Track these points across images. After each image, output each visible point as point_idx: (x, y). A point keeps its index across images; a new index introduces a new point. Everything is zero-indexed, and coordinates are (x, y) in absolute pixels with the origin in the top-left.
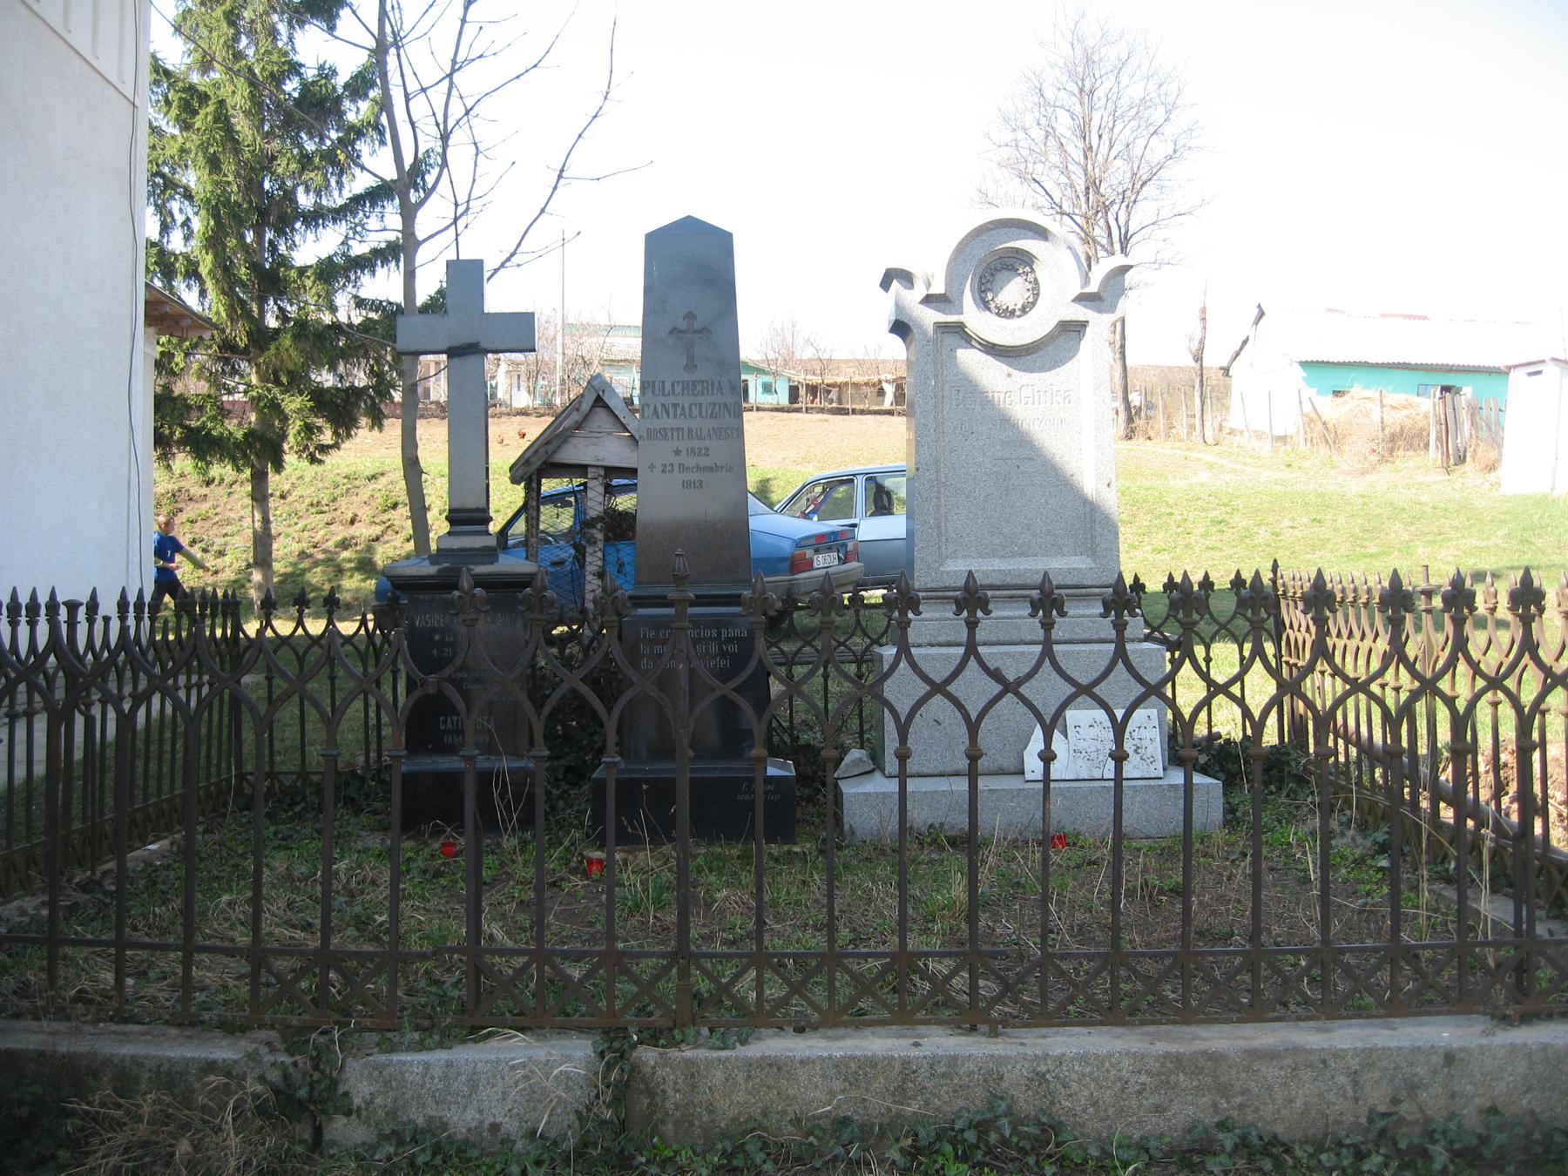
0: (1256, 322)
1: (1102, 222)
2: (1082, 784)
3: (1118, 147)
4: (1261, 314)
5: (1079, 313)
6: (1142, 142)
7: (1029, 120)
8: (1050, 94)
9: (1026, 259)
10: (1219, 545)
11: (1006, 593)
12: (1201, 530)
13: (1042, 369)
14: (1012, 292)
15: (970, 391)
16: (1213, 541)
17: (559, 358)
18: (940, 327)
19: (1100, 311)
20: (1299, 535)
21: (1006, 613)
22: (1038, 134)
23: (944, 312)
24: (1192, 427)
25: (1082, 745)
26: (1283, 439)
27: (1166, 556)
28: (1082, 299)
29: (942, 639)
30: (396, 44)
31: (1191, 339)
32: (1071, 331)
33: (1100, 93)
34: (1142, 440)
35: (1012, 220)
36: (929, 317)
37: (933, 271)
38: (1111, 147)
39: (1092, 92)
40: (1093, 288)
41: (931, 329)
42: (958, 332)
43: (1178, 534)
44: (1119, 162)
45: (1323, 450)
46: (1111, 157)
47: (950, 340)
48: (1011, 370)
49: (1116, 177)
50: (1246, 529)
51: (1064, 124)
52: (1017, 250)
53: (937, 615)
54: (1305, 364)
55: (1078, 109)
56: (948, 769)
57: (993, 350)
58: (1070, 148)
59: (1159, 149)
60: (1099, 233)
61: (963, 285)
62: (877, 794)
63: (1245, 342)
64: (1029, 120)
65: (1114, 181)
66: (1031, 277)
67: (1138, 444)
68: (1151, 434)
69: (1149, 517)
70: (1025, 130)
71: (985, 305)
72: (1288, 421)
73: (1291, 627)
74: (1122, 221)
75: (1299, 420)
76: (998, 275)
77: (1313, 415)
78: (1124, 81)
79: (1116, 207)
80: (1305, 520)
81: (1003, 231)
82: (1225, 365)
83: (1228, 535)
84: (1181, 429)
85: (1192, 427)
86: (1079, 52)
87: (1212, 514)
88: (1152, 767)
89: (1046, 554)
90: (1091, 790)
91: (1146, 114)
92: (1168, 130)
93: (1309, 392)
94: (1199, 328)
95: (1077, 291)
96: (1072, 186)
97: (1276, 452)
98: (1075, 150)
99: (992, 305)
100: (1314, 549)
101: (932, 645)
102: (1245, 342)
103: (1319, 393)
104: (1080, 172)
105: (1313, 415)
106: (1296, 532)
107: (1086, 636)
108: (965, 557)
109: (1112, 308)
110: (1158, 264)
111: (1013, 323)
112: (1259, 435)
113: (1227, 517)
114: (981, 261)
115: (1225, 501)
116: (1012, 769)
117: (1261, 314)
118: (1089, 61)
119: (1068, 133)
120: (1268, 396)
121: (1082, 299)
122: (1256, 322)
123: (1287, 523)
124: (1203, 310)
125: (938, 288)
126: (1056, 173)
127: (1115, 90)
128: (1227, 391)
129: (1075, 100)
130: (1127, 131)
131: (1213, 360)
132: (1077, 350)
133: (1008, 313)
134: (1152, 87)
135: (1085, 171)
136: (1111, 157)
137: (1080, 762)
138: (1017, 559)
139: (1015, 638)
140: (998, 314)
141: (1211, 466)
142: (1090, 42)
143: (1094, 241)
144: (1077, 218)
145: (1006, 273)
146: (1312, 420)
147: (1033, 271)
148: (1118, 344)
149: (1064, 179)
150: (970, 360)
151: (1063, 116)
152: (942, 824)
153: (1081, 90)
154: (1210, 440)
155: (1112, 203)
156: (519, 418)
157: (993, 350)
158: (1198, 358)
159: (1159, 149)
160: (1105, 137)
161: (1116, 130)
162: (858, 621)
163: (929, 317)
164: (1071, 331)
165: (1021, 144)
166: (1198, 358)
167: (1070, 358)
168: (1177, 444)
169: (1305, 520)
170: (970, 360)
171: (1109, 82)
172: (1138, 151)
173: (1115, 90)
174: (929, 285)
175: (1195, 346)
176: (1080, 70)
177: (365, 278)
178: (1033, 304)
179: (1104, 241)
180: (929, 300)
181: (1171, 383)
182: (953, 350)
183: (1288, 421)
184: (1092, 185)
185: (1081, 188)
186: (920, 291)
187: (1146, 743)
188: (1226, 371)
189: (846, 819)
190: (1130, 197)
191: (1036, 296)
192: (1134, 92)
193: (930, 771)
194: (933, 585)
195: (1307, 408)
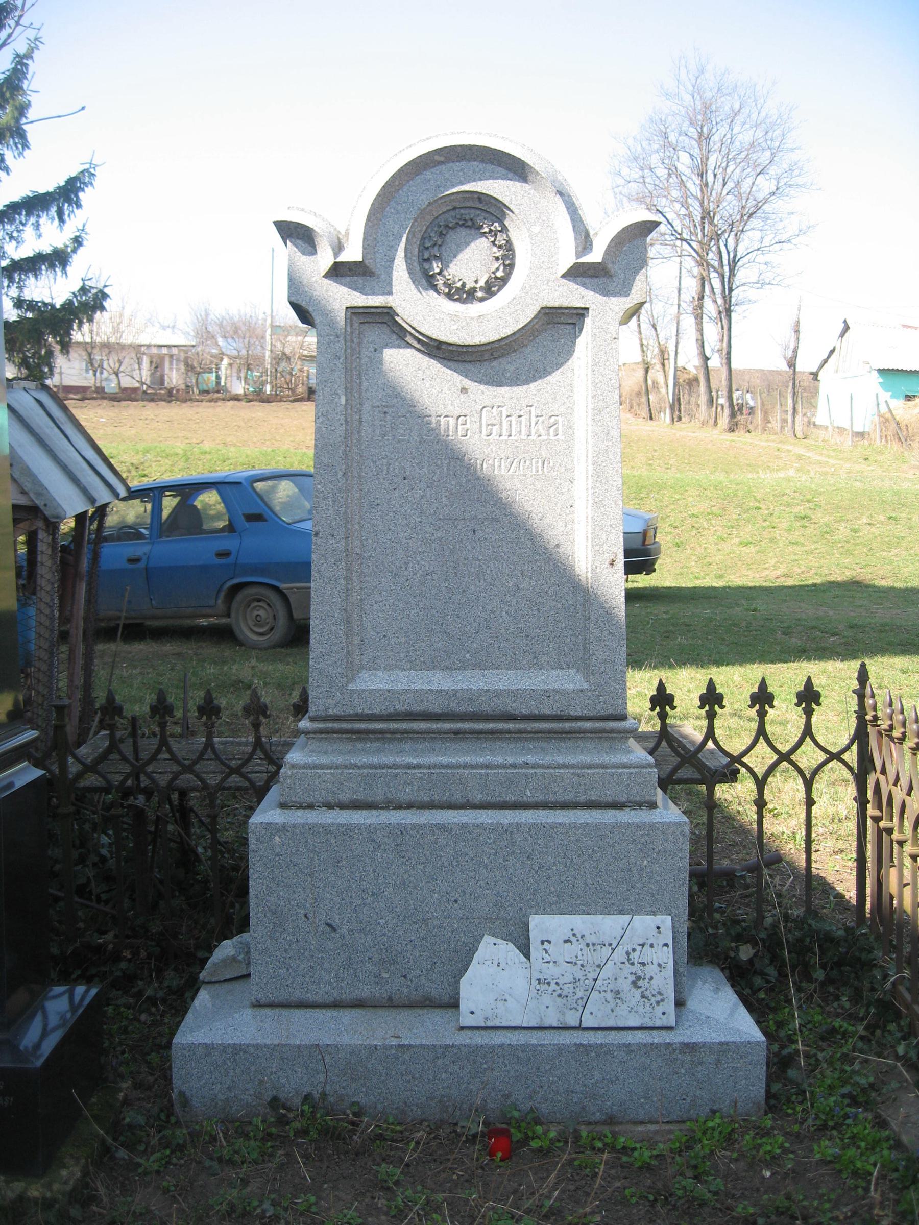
0: (842, 335)
1: (714, 249)
2: (547, 1038)
3: (730, 185)
4: (847, 328)
5: (574, 295)
6: (749, 181)
7: (654, 160)
8: (672, 138)
9: (494, 210)
10: (802, 540)
11: (448, 726)
12: (785, 525)
13: (517, 380)
14: (472, 261)
15: (401, 410)
16: (796, 536)
17: (268, 354)
18: (354, 312)
19: (606, 293)
20: (877, 532)
21: (444, 760)
22: (662, 172)
23: (362, 291)
24: (785, 421)
25: (551, 971)
26: (862, 435)
27: (752, 549)
28: (579, 273)
29: (345, 797)
30: (720, 313)
31: (786, 348)
32: (558, 326)
33: (716, 138)
34: (742, 432)
35: (471, 148)
36: (341, 298)
37: (345, 222)
38: (724, 185)
39: (708, 138)
40: (596, 256)
41: (341, 316)
42: (385, 319)
43: (764, 528)
44: (729, 197)
45: (896, 446)
46: (725, 192)
47: (373, 334)
48: (467, 383)
49: (729, 207)
50: (827, 526)
51: (684, 163)
52: (480, 197)
53: (339, 760)
54: (882, 372)
55: (696, 152)
56: (346, 997)
57: (436, 349)
58: (689, 185)
59: (765, 185)
60: (712, 257)
61: (393, 248)
62: (224, 1048)
63: (832, 352)
64: (654, 160)
65: (726, 214)
66: (501, 239)
67: (740, 437)
68: (751, 427)
69: (738, 511)
70: (651, 170)
71: (428, 281)
72: (865, 421)
73: (884, 772)
74: (731, 248)
75: (876, 419)
76: (452, 236)
77: (888, 416)
78: (737, 129)
79: (726, 235)
80: (882, 518)
81: (457, 166)
82: (814, 370)
83: (808, 532)
84: (775, 424)
85: (785, 421)
86: (698, 103)
87: (796, 510)
88: (659, 1010)
89: (514, 665)
90: (560, 1050)
91: (754, 156)
92: (773, 170)
93: (885, 396)
94: (793, 339)
95: (568, 259)
96: (690, 215)
97: (855, 446)
98: (694, 187)
99: (440, 282)
100: (890, 546)
101: (330, 806)
102: (832, 352)
103: (892, 397)
104: (696, 205)
105: (888, 416)
106: (873, 529)
107: (569, 797)
108: (388, 668)
109: (625, 290)
110: (761, 284)
111: (475, 309)
112: (841, 430)
113: (809, 513)
114: (422, 212)
115: (809, 497)
116: (446, 999)
117: (847, 328)
118: (707, 107)
119: (687, 172)
120: (850, 399)
121: (579, 273)
122: (842, 335)
123: (865, 520)
124: (798, 323)
125: (353, 253)
126: (677, 206)
127: (729, 136)
128: (815, 392)
129: (694, 143)
130: (738, 171)
131: (805, 365)
132: (570, 352)
133: (463, 294)
134: (760, 133)
135: (702, 204)
136: (725, 192)
137: (547, 1000)
138: (468, 673)
139: (458, 797)
140: (449, 296)
141: (800, 458)
142: (708, 95)
143: (708, 265)
144: (694, 244)
145: (462, 232)
146: (887, 420)
147: (504, 229)
148: (724, 352)
149: (683, 211)
150: (403, 364)
151: (684, 158)
152: (324, 1095)
153: (701, 134)
154: (799, 434)
155: (725, 231)
156: (231, 403)
157: (436, 349)
158: (792, 364)
159: (765, 185)
160: (720, 178)
161: (729, 170)
162: (258, 738)
163: (341, 298)
164: (558, 326)
165: (647, 180)
166: (792, 364)
167: (559, 365)
168: (772, 437)
169: (882, 518)
170: (403, 364)
171: (723, 129)
172: (745, 186)
173: (729, 136)
174: (338, 248)
175: (789, 354)
176: (699, 117)
177: (31, 281)
178: (504, 280)
179: (716, 264)
180: (338, 271)
181: (769, 384)
182: (378, 350)
183: (865, 421)
184: (707, 216)
185: (698, 219)
186: (325, 259)
187: (651, 970)
188: (815, 375)
189: (176, 1082)
190: (737, 227)
191: (509, 268)
192: (745, 137)
193: (318, 999)
194: (337, 711)
195: (883, 409)
